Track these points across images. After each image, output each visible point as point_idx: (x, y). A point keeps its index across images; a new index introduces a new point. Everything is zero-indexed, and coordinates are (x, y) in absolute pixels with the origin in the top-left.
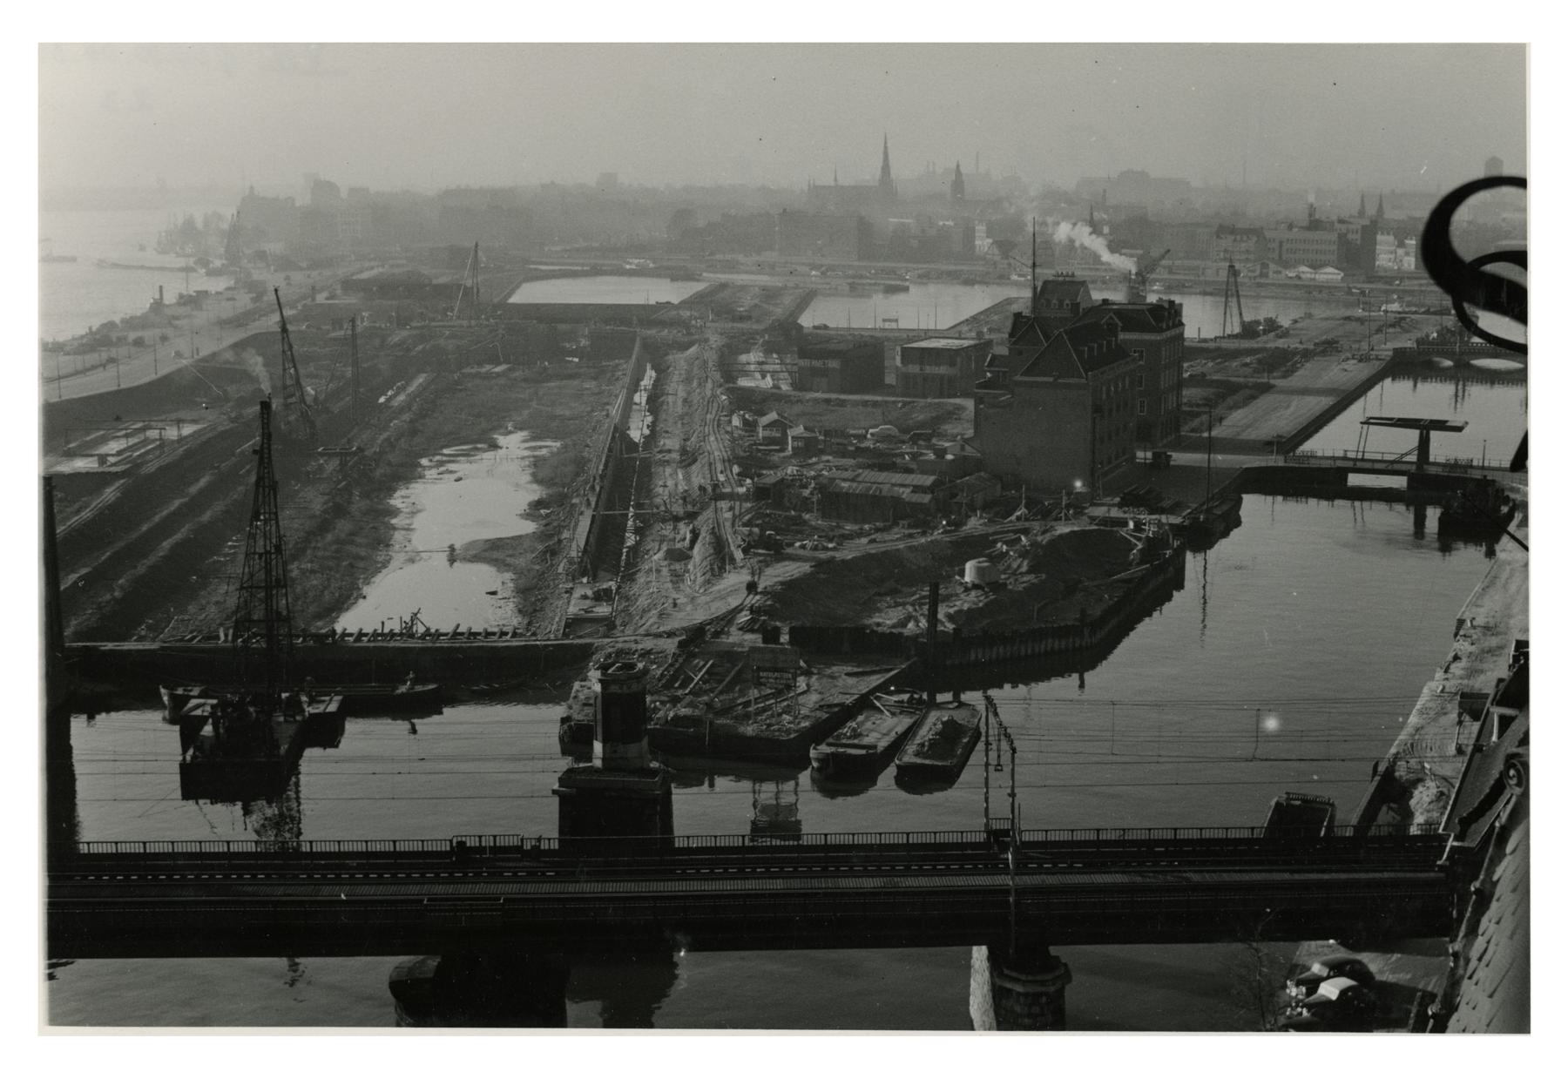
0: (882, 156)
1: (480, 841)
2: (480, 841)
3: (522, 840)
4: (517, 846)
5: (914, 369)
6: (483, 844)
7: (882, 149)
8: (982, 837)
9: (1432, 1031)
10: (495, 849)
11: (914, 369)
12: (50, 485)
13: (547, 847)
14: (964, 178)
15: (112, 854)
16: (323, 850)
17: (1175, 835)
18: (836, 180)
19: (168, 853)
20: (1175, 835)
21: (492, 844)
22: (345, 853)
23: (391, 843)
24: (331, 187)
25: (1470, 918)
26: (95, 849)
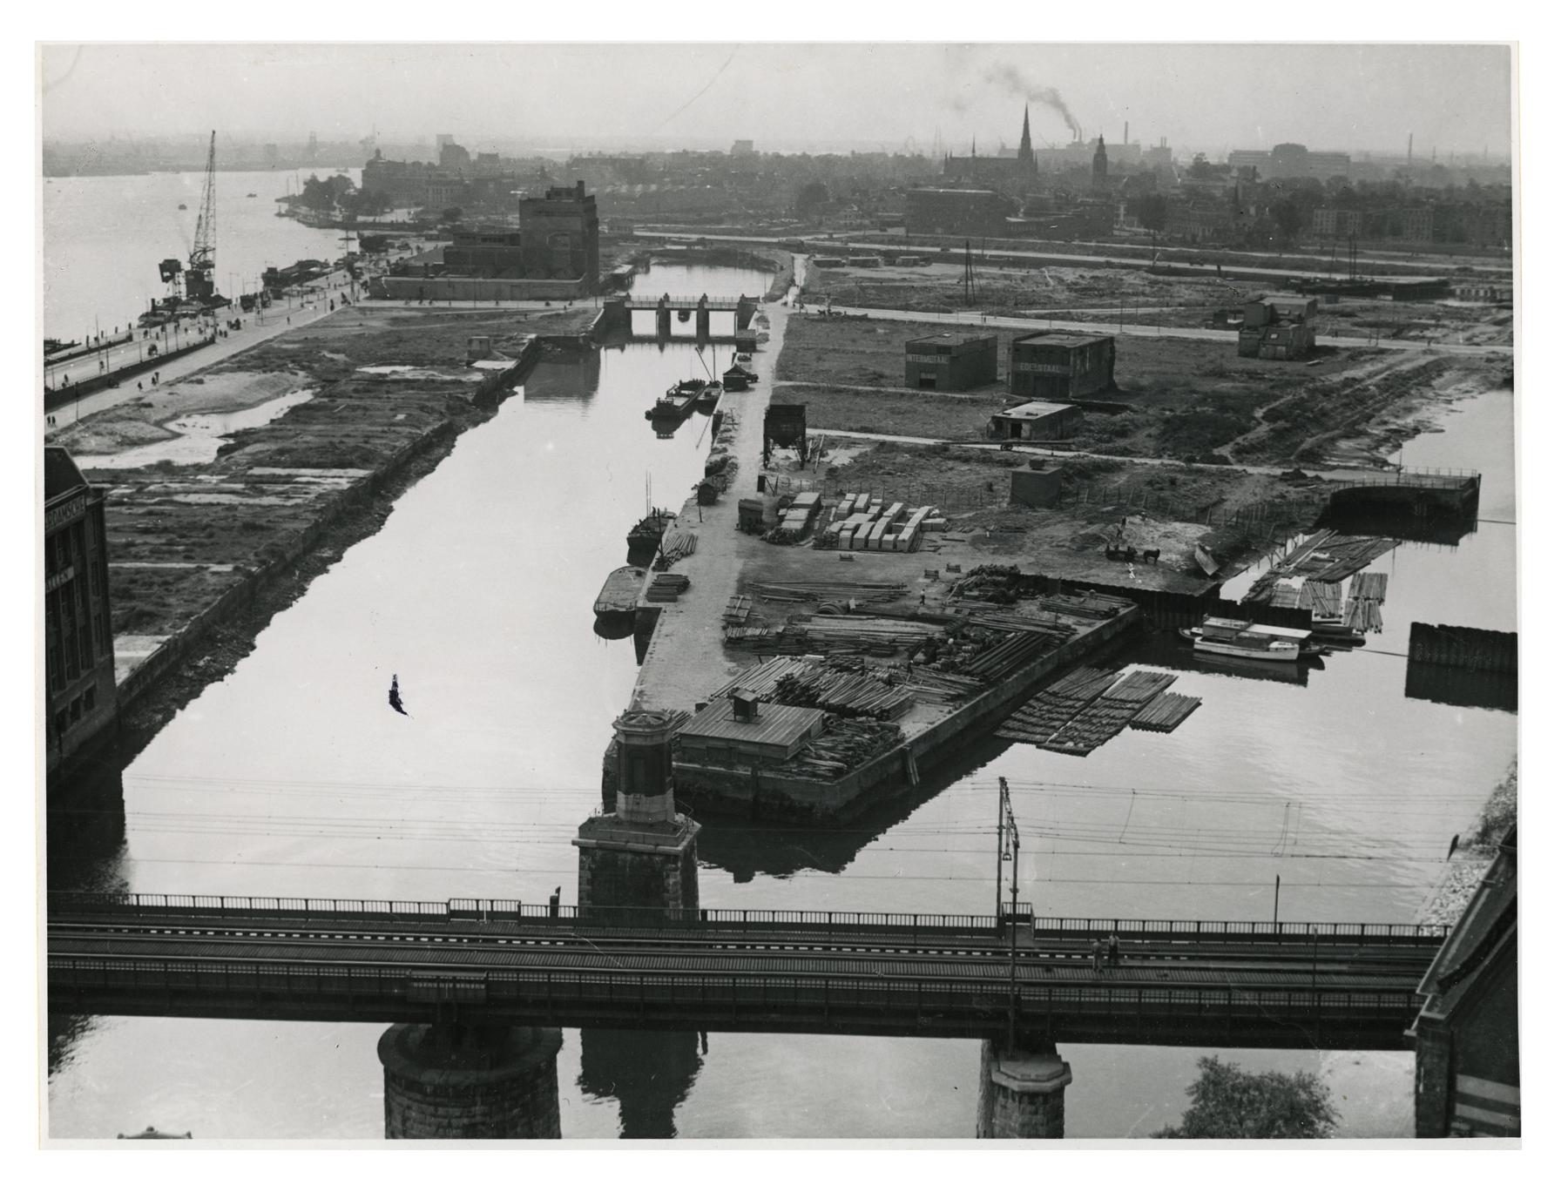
0: (1022, 127)
1: (915, 921)
2: (915, 921)
3: (519, 907)
4: (515, 912)
5: (1025, 367)
6: (481, 909)
7: (1023, 123)
8: (993, 924)
9: (1512, 1076)
10: (493, 915)
11: (1025, 367)
12: (46, 449)
13: (714, 919)
14: (1107, 152)
15: (797, 923)
16: (847, 922)
17: (1363, 931)
18: (974, 151)
19: (768, 923)
20: (1363, 931)
21: (489, 909)
22: (778, 923)
23: (827, 915)
24: (460, 151)
25: (1314, 260)
26: (144, 902)
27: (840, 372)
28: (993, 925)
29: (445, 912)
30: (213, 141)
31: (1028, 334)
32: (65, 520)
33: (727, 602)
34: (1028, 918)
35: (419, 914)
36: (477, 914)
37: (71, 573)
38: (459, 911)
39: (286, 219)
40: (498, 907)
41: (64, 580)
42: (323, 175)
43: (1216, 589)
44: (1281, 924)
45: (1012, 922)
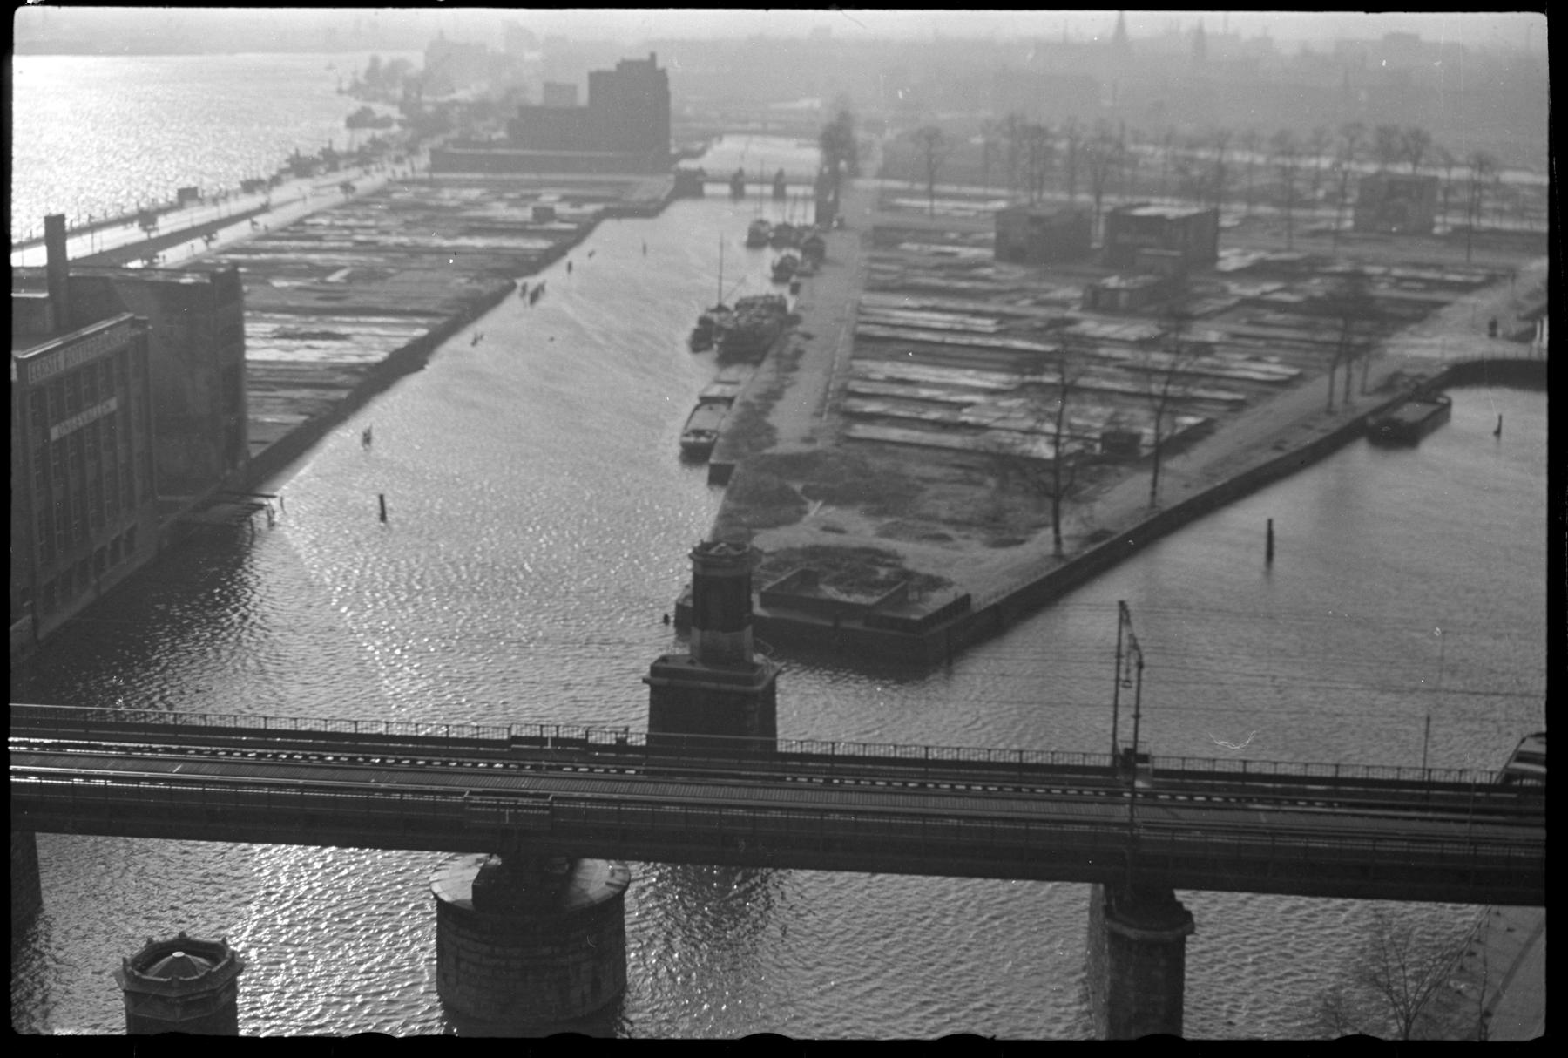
6: (545, 735)
8: (1107, 762)
27: (1483, 713)
28: (644, 742)
29: (505, 737)
30: (1154, 494)
31: (487, 225)
32: (108, 349)
33: (1511, 745)
34: (1145, 758)
35: (265, 730)
36: (541, 740)
37: (113, 404)
38: (521, 738)
39: (346, 97)
40: (564, 734)
41: (106, 412)
42: (386, 58)
43: (750, 536)
44: (1430, 770)
45: (1129, 761)
